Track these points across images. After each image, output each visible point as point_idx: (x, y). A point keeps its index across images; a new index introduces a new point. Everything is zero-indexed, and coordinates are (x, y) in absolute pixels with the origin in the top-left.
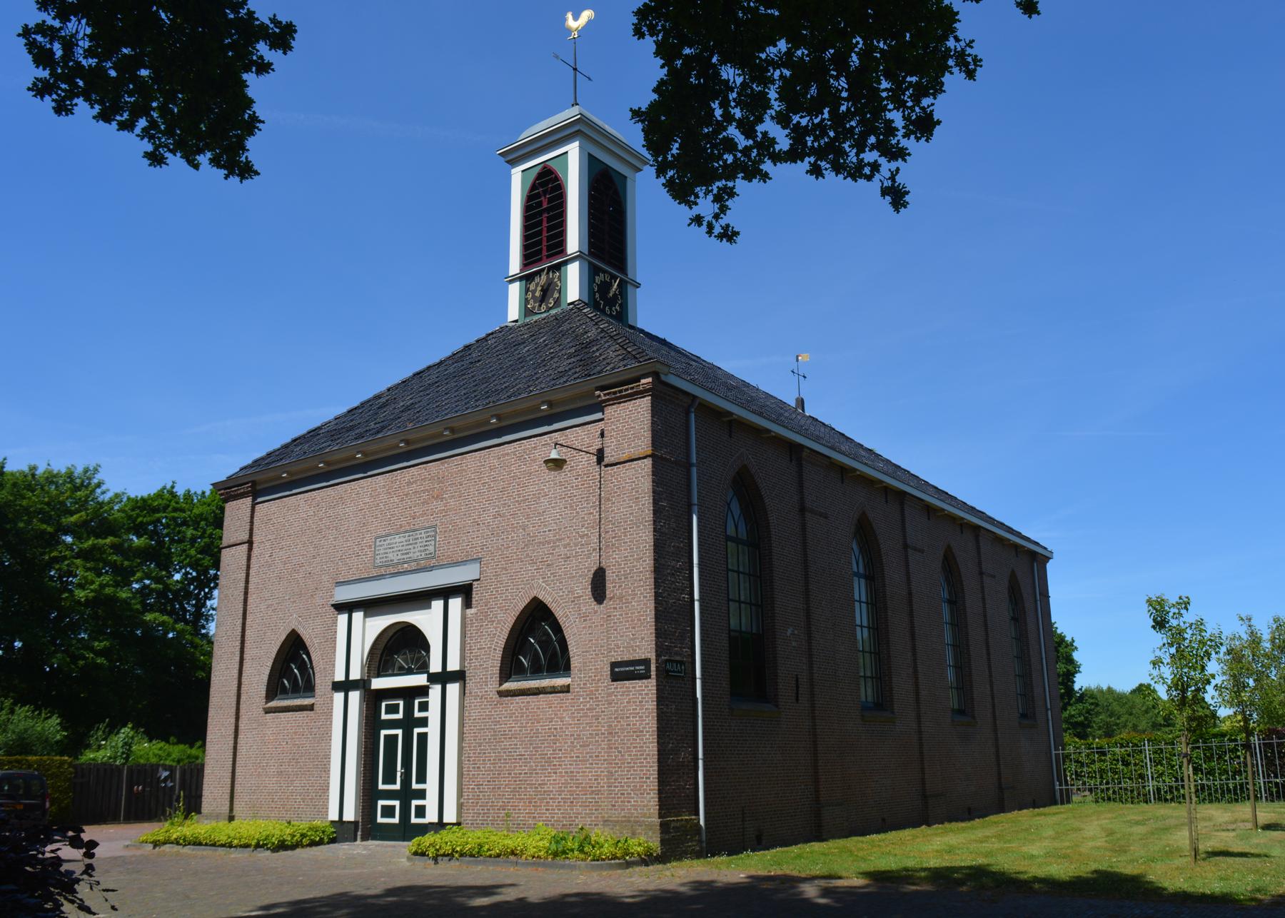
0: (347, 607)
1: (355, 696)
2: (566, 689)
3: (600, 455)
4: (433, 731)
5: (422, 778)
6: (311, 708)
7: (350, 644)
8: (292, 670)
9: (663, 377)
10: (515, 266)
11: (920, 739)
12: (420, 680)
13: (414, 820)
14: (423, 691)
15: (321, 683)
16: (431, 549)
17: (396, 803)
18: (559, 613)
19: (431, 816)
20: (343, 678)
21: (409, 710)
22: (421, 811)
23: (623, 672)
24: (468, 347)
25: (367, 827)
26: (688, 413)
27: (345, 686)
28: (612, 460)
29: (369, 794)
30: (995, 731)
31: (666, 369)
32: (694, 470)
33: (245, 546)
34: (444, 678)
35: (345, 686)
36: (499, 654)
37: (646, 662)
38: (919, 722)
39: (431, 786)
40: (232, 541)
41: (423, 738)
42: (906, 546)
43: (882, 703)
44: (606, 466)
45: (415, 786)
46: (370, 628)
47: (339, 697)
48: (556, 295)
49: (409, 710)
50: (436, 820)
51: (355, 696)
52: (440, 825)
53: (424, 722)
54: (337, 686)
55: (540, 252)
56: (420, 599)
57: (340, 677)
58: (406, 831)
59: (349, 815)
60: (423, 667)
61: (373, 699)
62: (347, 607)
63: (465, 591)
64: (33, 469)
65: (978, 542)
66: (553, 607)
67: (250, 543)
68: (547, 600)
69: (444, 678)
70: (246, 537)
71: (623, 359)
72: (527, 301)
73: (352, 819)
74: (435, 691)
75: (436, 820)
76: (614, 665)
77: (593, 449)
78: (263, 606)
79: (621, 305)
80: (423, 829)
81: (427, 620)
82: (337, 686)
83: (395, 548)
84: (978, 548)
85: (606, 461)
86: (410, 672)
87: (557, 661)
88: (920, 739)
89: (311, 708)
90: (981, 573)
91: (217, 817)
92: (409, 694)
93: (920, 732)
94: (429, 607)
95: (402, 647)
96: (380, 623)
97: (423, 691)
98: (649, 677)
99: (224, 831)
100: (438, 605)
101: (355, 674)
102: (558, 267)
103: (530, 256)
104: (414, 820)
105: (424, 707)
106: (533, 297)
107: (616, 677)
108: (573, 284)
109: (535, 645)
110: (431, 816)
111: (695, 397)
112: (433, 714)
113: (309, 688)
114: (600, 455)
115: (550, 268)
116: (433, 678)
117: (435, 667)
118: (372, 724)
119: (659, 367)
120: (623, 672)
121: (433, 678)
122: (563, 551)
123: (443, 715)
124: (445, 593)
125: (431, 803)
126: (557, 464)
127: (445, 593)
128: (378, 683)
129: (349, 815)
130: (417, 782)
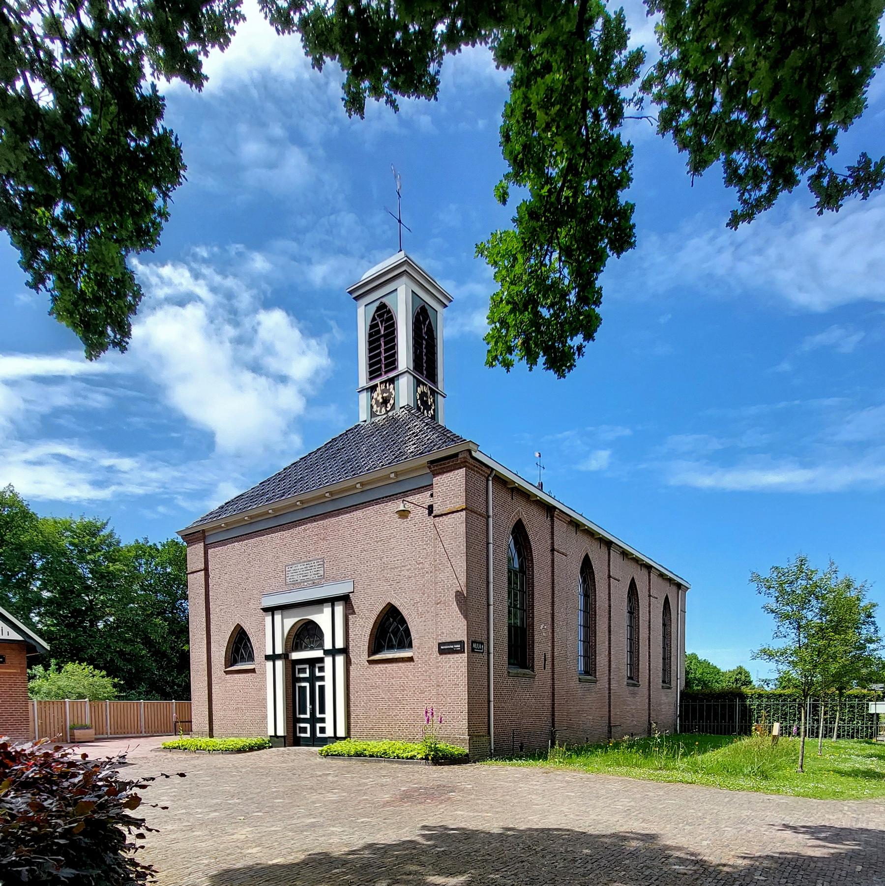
0: (271, 610)
1: (279, 664)
2: (411, 659)
3: (430, 509)
4: (328, 684)
5: (322, 711)
6: (253, 671)
7: (269, 636)
8: (240, 647)
9: (474, 454)
10: (363, 380)
11: (610, 693)
12: (319, 654)
13: (319, 735)
14: (321, 660)
15: (258, 656)
16: (322, 573)
17: (308, 726)
18: (405, 613)
19: (329, 733)
20: (271, 653)
21: (312, 672)
22: (323, 730)
23: (446, 649)
24: (334, 440)
25: (293, 739)
26: (488, 480)
27: (273, 658)
28: (439, 513)
29: (292, 720)
30: (649, 690)
31: (475, 448)
32: (491, 520)
33: (203, 572)
34: (333, 652)
35: (273, 658)
36: (367, 638)
37: (461, 643)
38: (609, 684)
39: (328, 715)
40: (194, 570)
41: (322, 688)
42: (609, 577)
43: (590, 669)
44: (434, 517)
45: (318, 715)
46: (287, 623)
47: (270, 664)
48: (392, 402)
49: (312, 672)
50: (332, 735)
51: (279, 664)
52: (336, 738)
53: (322, 679)
54: (268, 658)
55: (380, 369)
56: (320, 602)
57: (269, 652)
58: (314, 741)
59: (281, 732)
60: (321, 646)
61: (292, 667)
62: (271, 610)
63: (345, 599)
64: (185, 168)
65: (649, 576)
66: (401, 609)
67: (206, 569)
68: (397, 604)
69: (333, 652)
70: (203, 566)
71: (445, 442)
72: (372, 407)
73: (282, 734)
74: (328, 660)
75: (332, 735)
76: (440, 644)
77: (426, 505)
78: (218, 610)
79: (434, 410)
80: (324, 741)
81: (322, 618)
82: (268, 658)
83: (297, 573)
84: (650, 580)
85: (435, 513)
86: (312, 649)
87: (404, 639)
88: (610, 693)
89: (253, 671)
90: (650, 596)
91: (202, 734)
92: (312, 662)
93: (610, 689)
94: (322, 612)
95: (307, 634)
96: (290, 622)
97: (321, 660)
98: (464, 652)
99: (204, 741)
100: (327, 610)
101: (279, 651)
102: (392, 381)
103: (373, 373)
104: (319, 735)
105: (322, 669)
106: (377, 401)
107: (442, 652)
108: (404, 391)
109: (391, 631)
110: (329, 733)
111: (493, 469)
112: (328, 673)
113: (251, 658)
114: (430, 509)
115: (385, 382)
116: (327, 652)
117: (328, 645)
118: (292, 680)
119: (471, 446)
120: (446, 649)
121: (327, 652)
122: (407, 573)
123: (332, 673)
124: (332, 601)
125: (329, 725)
126: (404, 514)
127: (332, 601)
128: (295, 656)
129: (281, 732)
130: (320, 713)
